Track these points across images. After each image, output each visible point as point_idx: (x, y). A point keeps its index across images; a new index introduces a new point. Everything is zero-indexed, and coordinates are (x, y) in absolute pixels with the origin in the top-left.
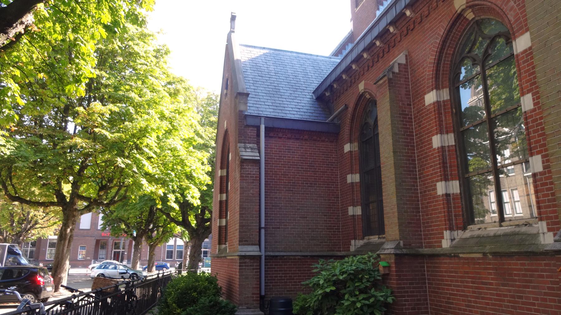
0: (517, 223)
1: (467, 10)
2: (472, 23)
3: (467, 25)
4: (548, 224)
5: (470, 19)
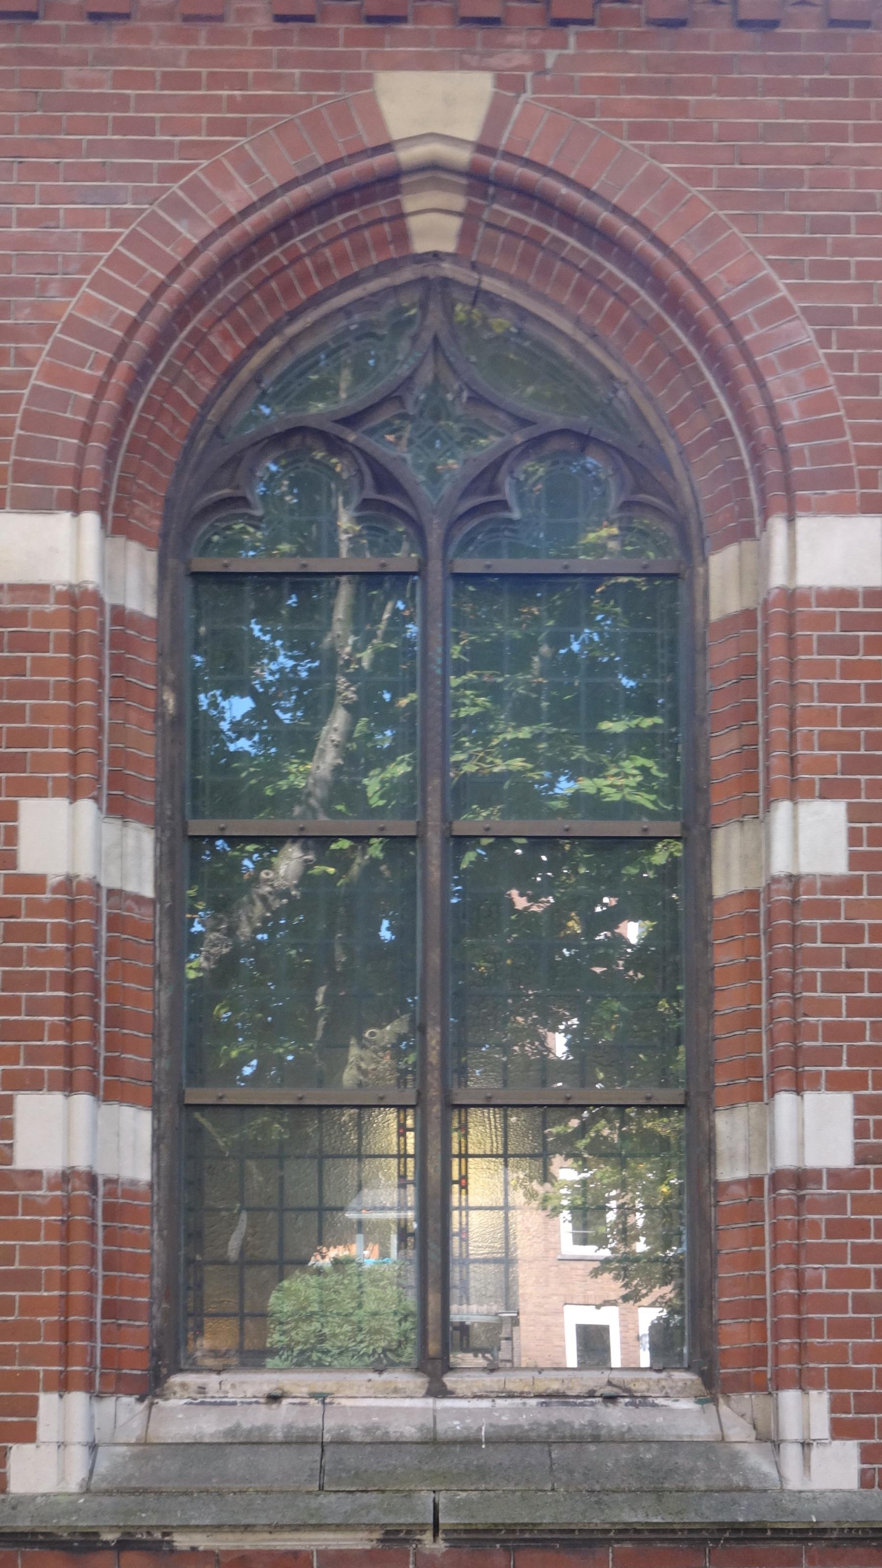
0: (555, 1386)
1: (440, 186)
2: (407, 274)
3: (379, 270)
4: (837, 1405)
5: (420, 246)
